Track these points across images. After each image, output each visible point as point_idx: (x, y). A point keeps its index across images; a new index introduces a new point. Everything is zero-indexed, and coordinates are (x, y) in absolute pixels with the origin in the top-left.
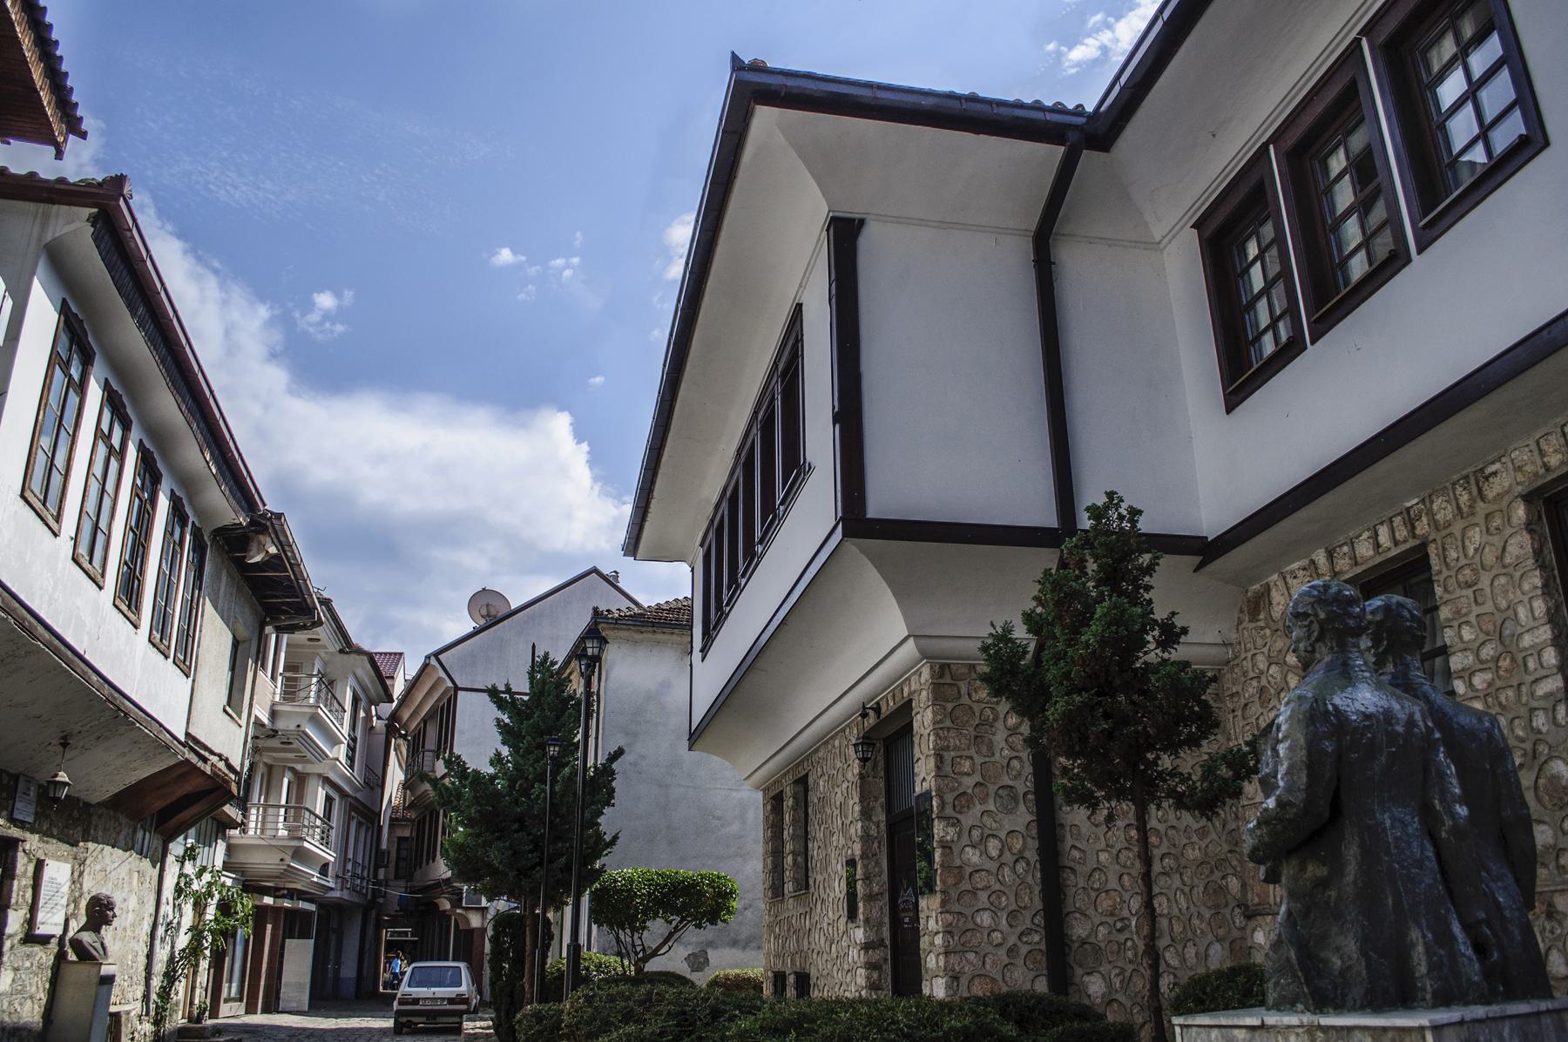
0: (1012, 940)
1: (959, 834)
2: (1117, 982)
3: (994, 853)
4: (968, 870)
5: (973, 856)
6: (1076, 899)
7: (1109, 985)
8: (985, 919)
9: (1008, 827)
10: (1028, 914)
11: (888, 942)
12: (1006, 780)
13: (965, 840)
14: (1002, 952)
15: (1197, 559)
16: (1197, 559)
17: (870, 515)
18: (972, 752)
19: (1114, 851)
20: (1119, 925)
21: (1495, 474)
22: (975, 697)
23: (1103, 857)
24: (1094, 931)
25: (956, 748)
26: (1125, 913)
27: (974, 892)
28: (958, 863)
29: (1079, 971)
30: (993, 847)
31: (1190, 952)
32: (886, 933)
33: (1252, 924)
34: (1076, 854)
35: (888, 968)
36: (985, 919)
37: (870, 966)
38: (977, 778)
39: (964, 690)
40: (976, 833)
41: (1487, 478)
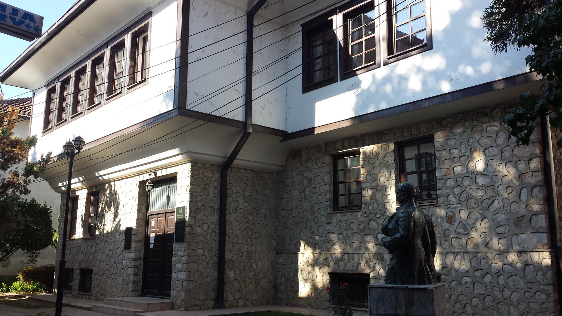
0: (208, 259)
1: (195, 223)
2: (238, 273)
3: (205, 229)
4: (197, 234)
5: (199, 230)
6: (228, 246)
7: (235, 275)
8: (200, 252)
9: (211, 221)
10: (214, 250)
11: (142, 258)
12: (212, 205)
13: (197, 225)
14: (205, 263)
15: (282, 138)
16: (282, 138)
17: (188, 108)
18: (202, 194)
19: (241, 230)
20: (241, 255)
21: (387, 134)
22: (205, 175)
23: (238, 232)
24: (233, 257)
25: (197, 192)
26: (243, 251)
27: (198, 242)
28: (194, 232)
29: (227, 270)
30: (205, 226)
31: (260, 264)
32: (142, 254)
33: (279, 255)
34: (230, 231)
35: (141, 268)
36: (200, 252)
37: (136, 267)
38: (202, 203)
39: (201, 172)
40: (200, 222)
41: (384, 134)
